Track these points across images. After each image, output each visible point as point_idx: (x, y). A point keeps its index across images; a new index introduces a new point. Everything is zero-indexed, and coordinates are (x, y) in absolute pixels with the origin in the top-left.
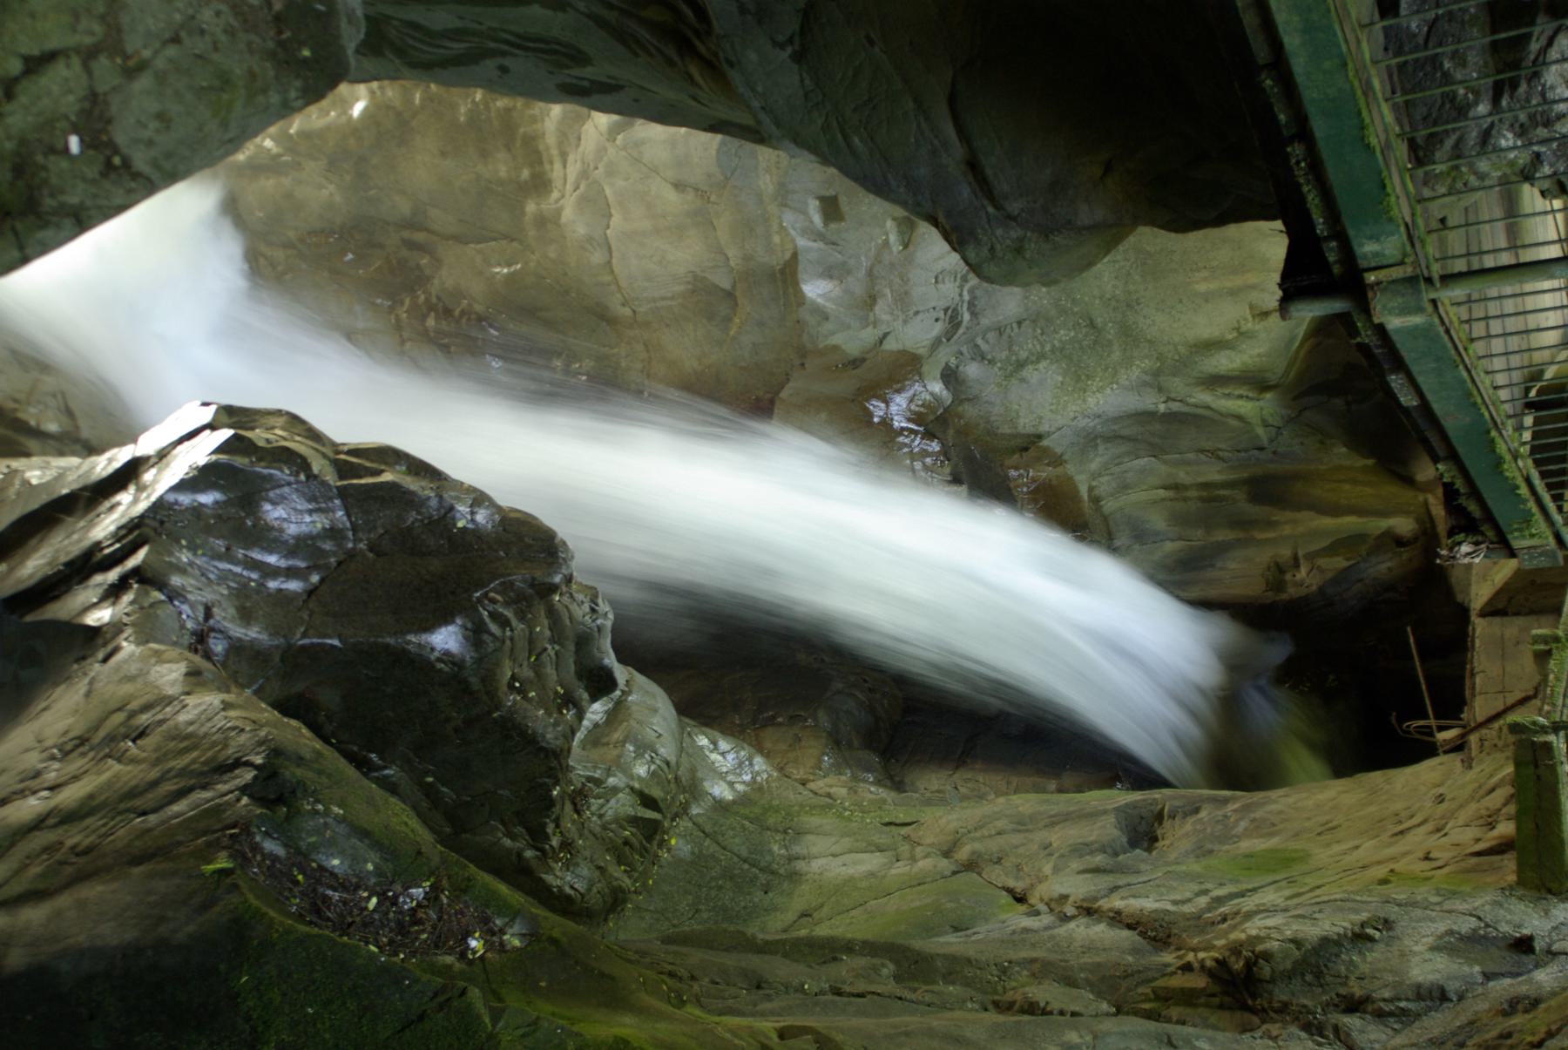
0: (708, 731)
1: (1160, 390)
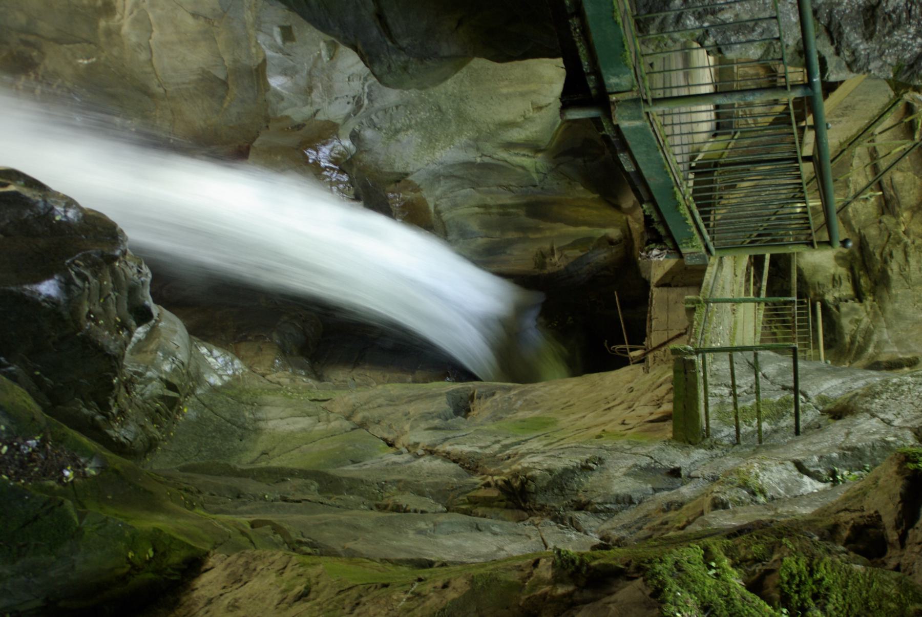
0: (207, 344)
1: (478, 149)
